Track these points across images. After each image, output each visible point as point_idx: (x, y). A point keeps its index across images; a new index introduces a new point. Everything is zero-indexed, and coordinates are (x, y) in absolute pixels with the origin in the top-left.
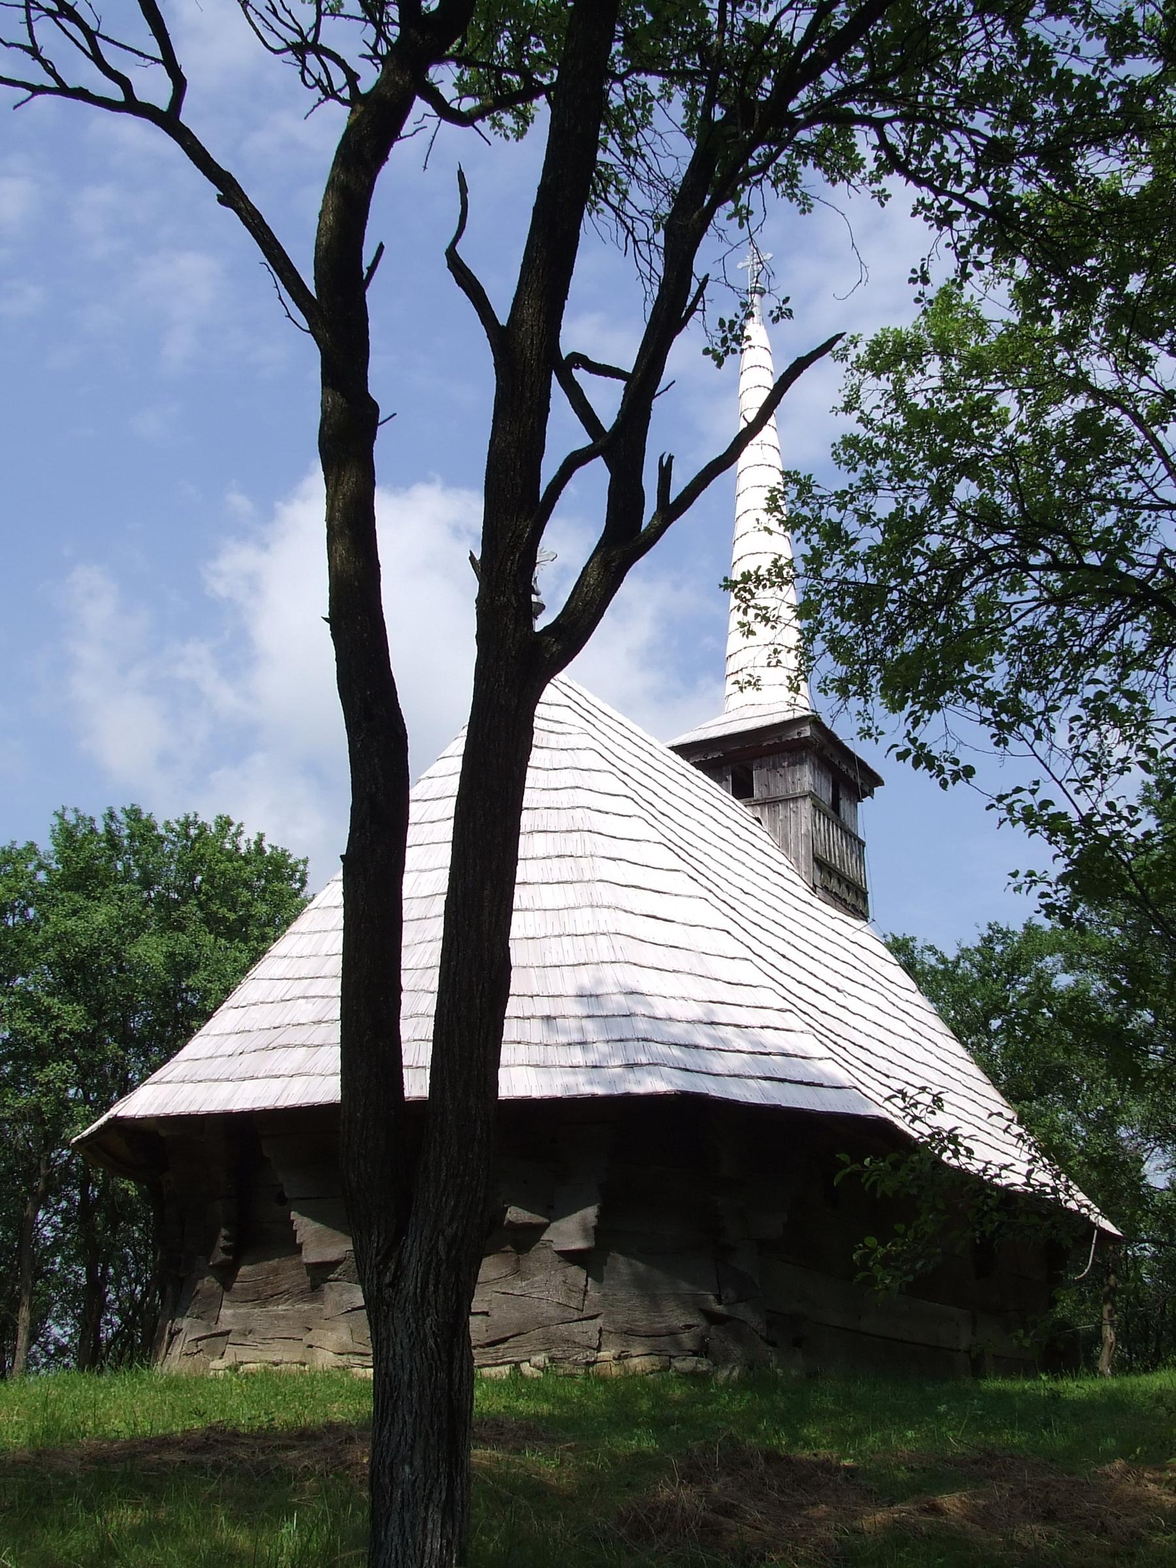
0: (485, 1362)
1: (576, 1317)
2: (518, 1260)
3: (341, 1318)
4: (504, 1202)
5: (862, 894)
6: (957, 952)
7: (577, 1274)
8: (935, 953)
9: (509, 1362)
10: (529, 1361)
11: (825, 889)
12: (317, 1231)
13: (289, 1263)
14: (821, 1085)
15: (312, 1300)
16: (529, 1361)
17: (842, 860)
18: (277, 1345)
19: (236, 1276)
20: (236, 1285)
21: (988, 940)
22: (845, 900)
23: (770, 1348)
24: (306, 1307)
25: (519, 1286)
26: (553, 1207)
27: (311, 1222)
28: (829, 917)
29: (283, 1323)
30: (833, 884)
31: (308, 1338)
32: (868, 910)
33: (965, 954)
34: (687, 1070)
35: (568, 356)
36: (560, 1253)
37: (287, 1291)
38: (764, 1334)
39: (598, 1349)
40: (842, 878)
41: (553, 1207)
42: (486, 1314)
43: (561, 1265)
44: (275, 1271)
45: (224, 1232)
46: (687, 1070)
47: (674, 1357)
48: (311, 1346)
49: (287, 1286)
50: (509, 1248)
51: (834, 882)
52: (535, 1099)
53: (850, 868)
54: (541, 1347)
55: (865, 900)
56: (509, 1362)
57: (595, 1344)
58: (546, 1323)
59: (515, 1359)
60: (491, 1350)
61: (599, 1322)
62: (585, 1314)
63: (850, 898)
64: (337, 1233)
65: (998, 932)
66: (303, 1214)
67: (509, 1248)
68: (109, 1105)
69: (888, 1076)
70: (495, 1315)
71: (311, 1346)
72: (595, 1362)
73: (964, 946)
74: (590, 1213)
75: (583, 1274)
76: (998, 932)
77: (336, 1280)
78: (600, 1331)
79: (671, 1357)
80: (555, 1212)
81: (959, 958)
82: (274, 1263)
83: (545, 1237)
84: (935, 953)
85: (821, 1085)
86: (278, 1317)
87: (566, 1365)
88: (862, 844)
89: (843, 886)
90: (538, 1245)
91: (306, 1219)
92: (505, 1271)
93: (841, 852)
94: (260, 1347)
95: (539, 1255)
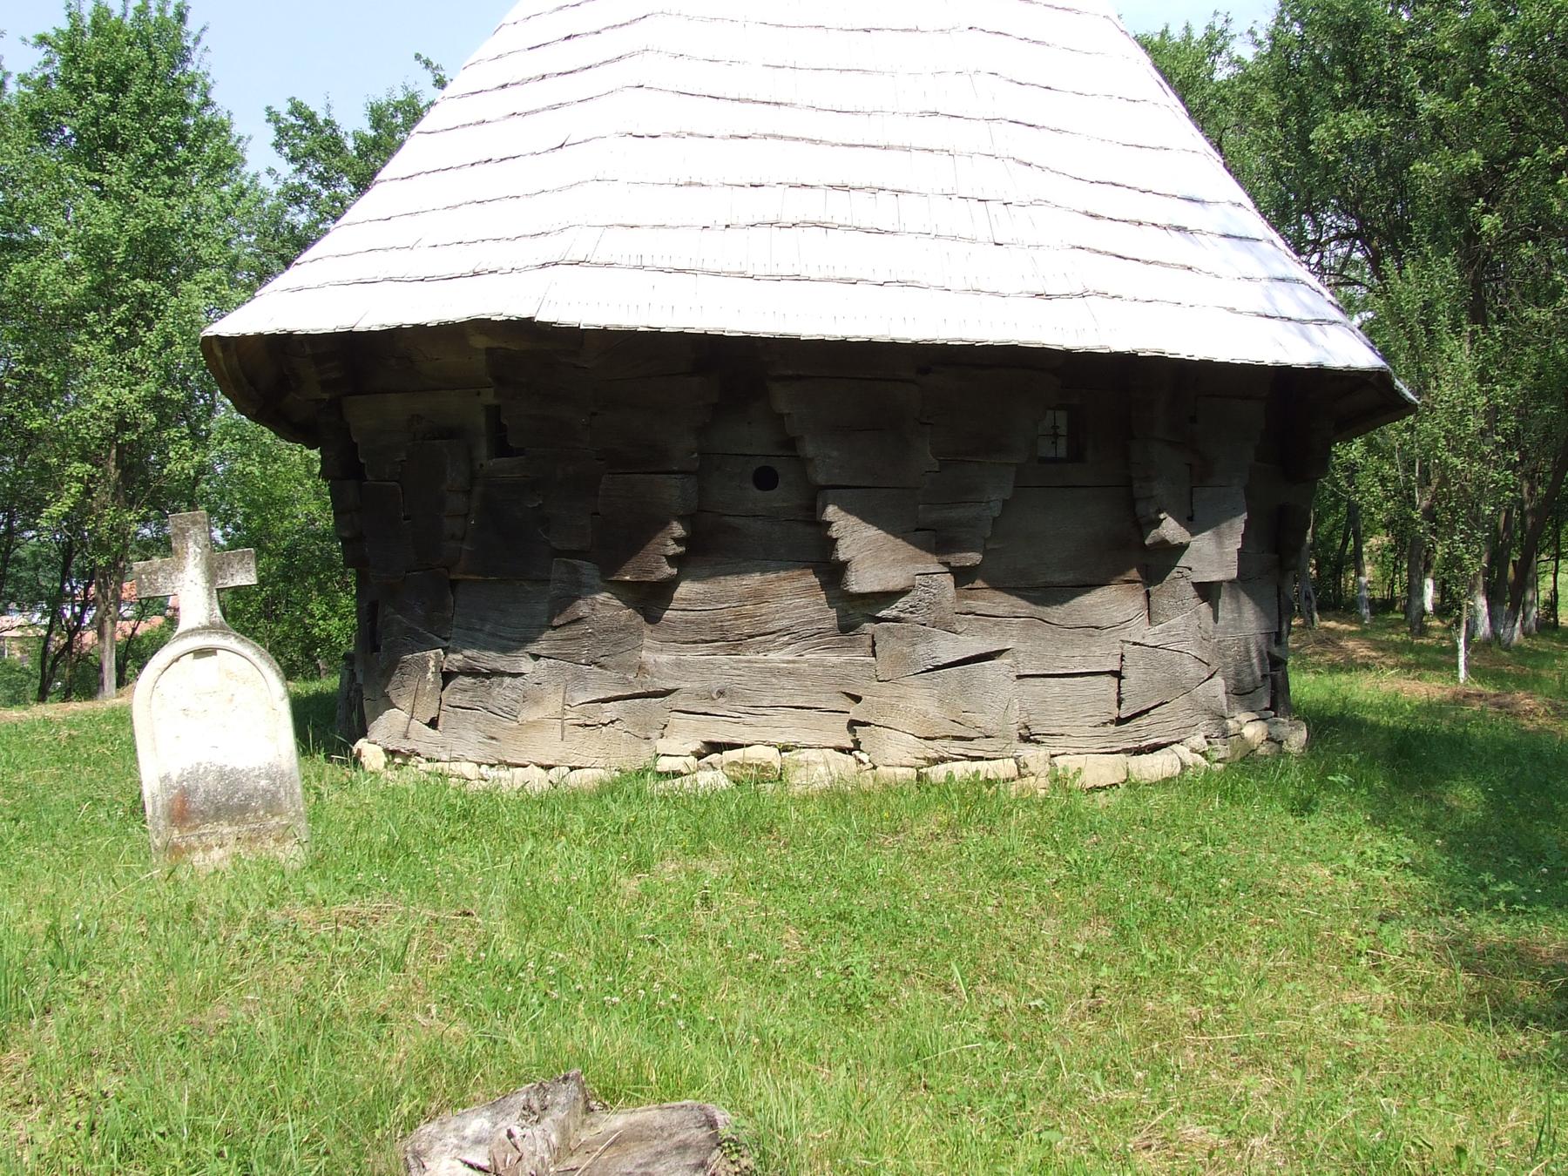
3: (916, 681)
13: (786, 585)
18: (779, 716)
19: (671, 599)
20: (668, 614)
24: (832, 658)
29: (788, 683)
35: (316, 448)
37: (786, 631)
44: (758, 597)
45: (678, 530)
49: (785, 623)
50: (1134, 574)
67: (1134, 574)
68: (137, 808)
74: (1245, 516)
77: (896, 620)
82: (754, 580)
83: (1182, 562)
86: (775, 672)
90: (1174, 573)
91: (853, 520)
94: (749, 719)
95: (1178, 586)
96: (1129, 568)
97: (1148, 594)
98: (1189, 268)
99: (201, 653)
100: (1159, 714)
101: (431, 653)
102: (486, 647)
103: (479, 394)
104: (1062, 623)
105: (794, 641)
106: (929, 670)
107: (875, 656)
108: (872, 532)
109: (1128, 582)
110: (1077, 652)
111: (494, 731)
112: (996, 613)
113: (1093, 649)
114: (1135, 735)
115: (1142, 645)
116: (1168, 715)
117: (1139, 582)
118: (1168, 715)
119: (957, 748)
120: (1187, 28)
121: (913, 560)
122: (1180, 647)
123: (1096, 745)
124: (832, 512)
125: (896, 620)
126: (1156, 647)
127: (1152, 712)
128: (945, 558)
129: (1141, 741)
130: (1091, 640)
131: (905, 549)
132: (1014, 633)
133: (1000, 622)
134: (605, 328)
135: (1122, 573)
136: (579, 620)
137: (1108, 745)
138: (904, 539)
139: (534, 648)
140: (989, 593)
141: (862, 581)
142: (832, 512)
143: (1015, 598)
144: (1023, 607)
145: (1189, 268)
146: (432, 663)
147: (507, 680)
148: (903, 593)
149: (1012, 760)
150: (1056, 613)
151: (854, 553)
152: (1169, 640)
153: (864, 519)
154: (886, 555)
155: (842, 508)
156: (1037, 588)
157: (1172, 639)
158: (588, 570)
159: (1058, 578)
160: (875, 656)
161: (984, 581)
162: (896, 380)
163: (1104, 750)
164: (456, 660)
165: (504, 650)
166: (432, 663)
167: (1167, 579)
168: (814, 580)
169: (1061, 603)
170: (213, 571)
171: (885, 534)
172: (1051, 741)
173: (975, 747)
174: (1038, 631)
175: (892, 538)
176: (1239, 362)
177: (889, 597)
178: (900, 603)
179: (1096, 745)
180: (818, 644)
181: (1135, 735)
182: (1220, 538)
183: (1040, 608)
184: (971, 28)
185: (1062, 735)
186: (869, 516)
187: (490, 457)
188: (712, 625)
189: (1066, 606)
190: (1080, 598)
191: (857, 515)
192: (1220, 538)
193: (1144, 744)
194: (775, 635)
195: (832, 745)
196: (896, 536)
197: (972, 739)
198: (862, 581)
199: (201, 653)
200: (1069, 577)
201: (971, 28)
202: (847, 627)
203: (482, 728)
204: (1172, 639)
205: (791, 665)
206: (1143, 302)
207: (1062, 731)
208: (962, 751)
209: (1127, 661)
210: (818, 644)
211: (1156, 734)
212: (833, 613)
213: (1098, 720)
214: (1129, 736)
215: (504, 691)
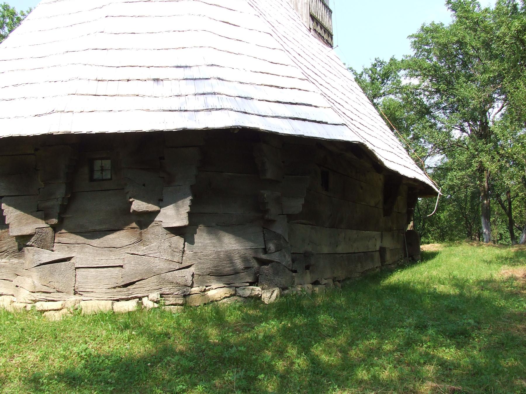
0: (121, 297)
1: (177, 268)
2: (141, 233)
4: (130, 198)
5: (331, 35)
6: (362, 70)
7: (178, 241)
8: (352, 71)
9: (136, 298)
10: (148, 296)
11: (315, 30)
12: (17, 216)
14: (326, 123)
15: (19, 257)
16: (148, 296)
17: (322, 18)
21: (375, 65)
22: (323, 37)
23: (294, 274)
25: (141, 249)
26: (162, 200)
27: (14, 210)
28: (317, 44)
30: (318, 29)
31: (17, 281)
32: (333, 43)
33: (366, 71)
34: (246, 113)
36: (167, 228)
38: (290, 268)
39: (192, 286)
40: (322, 27)
41: (162, 200)
42: (122, 266)
43: (168, 236)
46: (246, 113)
47: (238, 287)
48: (17, 286)
49: (6, 248)
50: (134, 225)
51: (319, 27)
52: (145, 133)
53: (326, 22)
54: (155, 288)
55: (332, 38)
56: (136, 298)
57: (190, 283)
58: (158, 272)
59: (139, 295)
60: (125, 289)
61: (192, 269)
62: (184, 265)
63: (326, 37)
64: (30, 216)
65: (379, 62)
66: (9, 205)
67: (134, 225)
69: (352, 120)
70: (127, 268)
71: (17, 286)
72: (189, 295)
73: (365, 67)
74: (190, 198)
75: (182, 240)
76: (379, 62)
77: (31, 246)
78: (193, 275)
79: (236, 287)
80: (161, 202)
81: (362, 73)
83: (157, 219)
84: (352, 71)
85: (326, 123)
87: (171, 299)
88: (331, 11)
89: (323, 30)
90: (153, 224)
91: (11, 208)
92: (134, 240)
93: (322, 13)
96: (132, 222)
98: (137, 95)
100: (141, 284)
104: (98, 246)
105: (8, 255)
106: (38, 266)
108: (18, 212)
109: (132, 228)
110: (103, 258)
112: (69, 242)
113: (111, 256)
114: (126, 292)
115: (137, 255)
116: (144, 284)
117: (137, 228)
118: (144, 284)
119: (43, 296)
121: (34, 222)
122: (155, 255)
123: (106, 297)
124: (4, 206)
126: (144, 255)
127: (137, 283)
128: (47, 221)
129: (129, 295)
130: (111, 253)
131: (31, 218)
132: (76, 250)
133: (71, 246)
134: (368, 147)
135: (128, 224)
137: (112, 296)
138: (31, 215)
140: (68, 234)
142: (4, 206)
143: (79, 236)
144: (81, 239)
145: (137, 95)
150: (96, 242)
151: (10, 221)
152: (149, 252)
153: (15, 208)
154: (24, 221)
155: (7, 204)
156: (89, 232)
157: (152, 252)
159: (98, 228)
161: (66, 230)
162: (26, 154)
163: (111, 299)
167: (150, 226)
169: (99, 238)
171: (24, 213)
172: (86, 294)
173: (51, 296)
174: (87, 250)
175: (27, 214)
176: (124, 132)
179: (106, 297)
180: (14, 256)
181: (126, 292)
182: (178, 209)
183: (89, 240)
184: (107, 17)
185: (92, 292)
186: (17, 207)
188: (199, 260)
189: (101, 239)
190: (108, 236)
191: (12, 207)
192: (178, 209)
193: (130, 297)
194: (3, 253)
195: (10, 294)
196: (29, 214)
197: (50, 293)
200: (104, 227)
201: (107, 17)
204: (152, 252)
205: (5, 264)
206: (87, 112)
207: (91, 290)
208: (44, 297)
210: (14, 256)
211: (137, 292)
212: (17, 244)
213: (110, 286)
214: (124, 293)
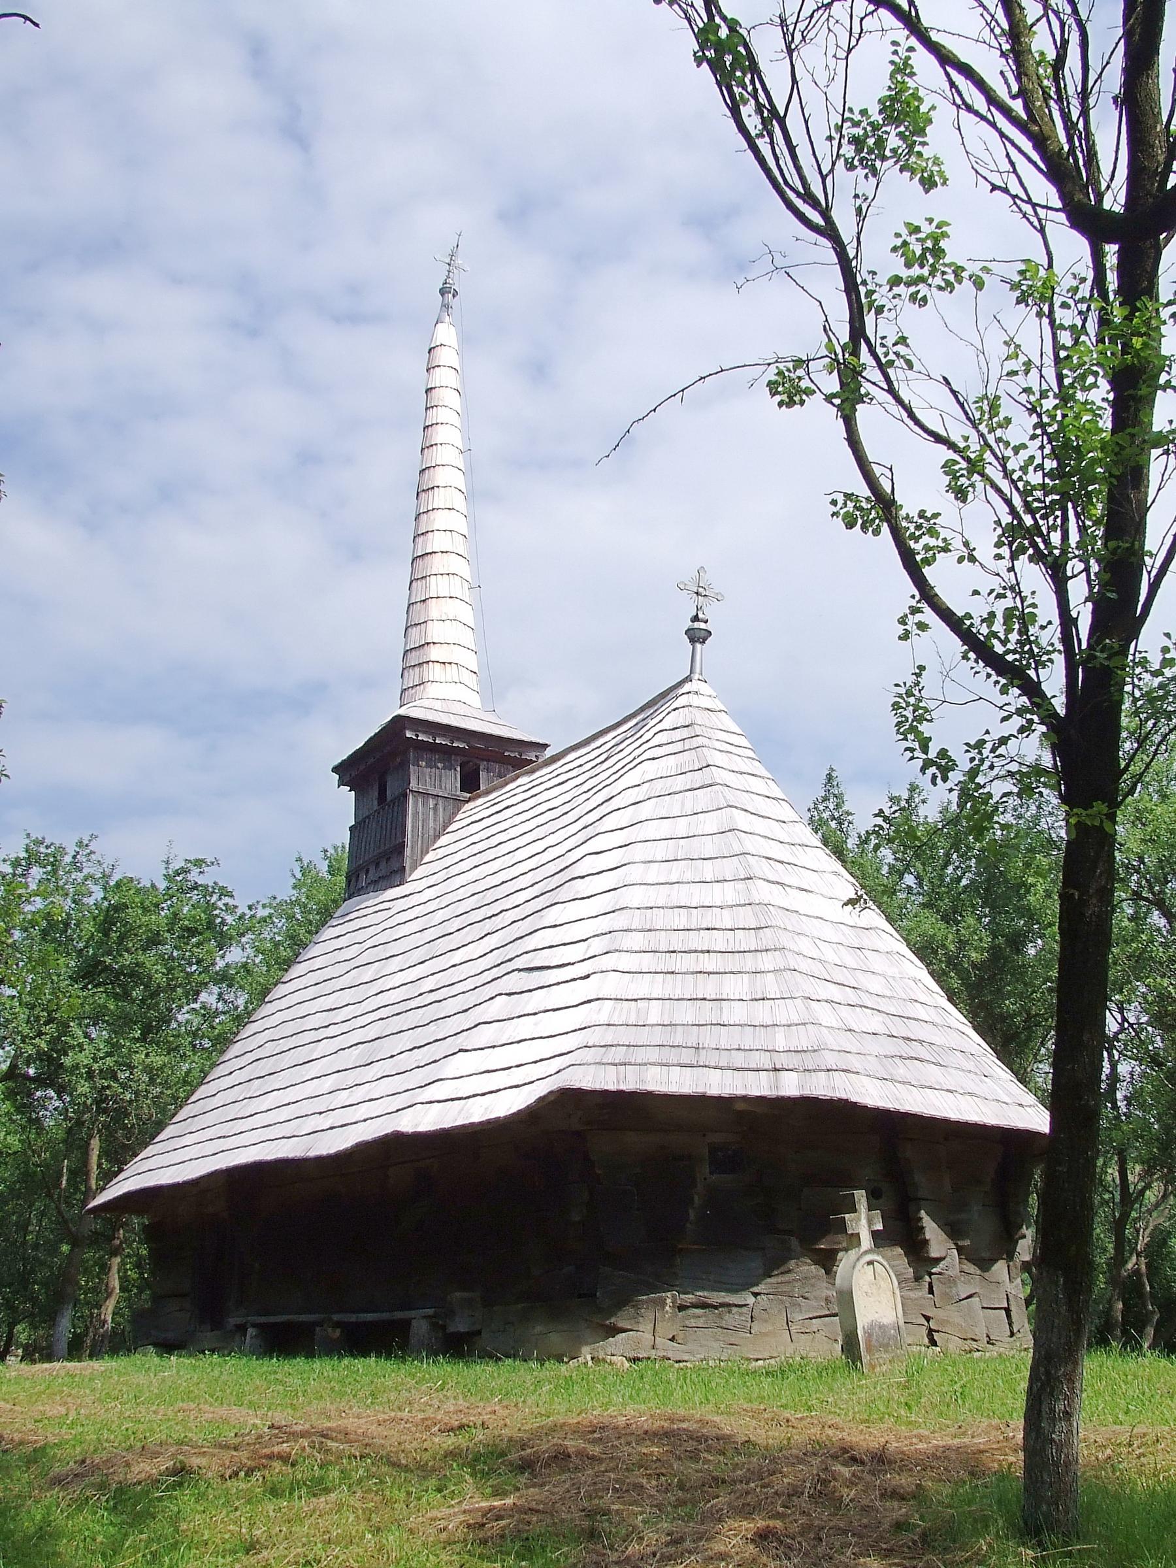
3: (952, 1307)
97: (1008, 1266)
99: (870, 1263)
101: (669, 1294)
102: (713, 1289)
103: (704, 1135)
107: (933, 1294)
111: (733, 1340)
120: (911, 179)
125: (940, 1274)
136: (789, 1271)
139: (755, 1289)
141: (934, 1253)
146: (669, 1301)
147: (735, 1310)
148: (944, 1258)
149: (1003, 1312)
158: (794, 1242)
160: (933, 1294)
164: (689, 1298)
165: (736, 1291)
166: (669, 1301)
168: (900, 1250)
170: (870, 1222)
177: (938, 1260)
178: (942, 1264)
187: (711, 1173)
198: (934, 1252)
199: (870, 1263)
202: (918, 1278)
203: (721, 1338)
209: (1011, 1303)
212: (911, 1270)
215: (732, 1318)
